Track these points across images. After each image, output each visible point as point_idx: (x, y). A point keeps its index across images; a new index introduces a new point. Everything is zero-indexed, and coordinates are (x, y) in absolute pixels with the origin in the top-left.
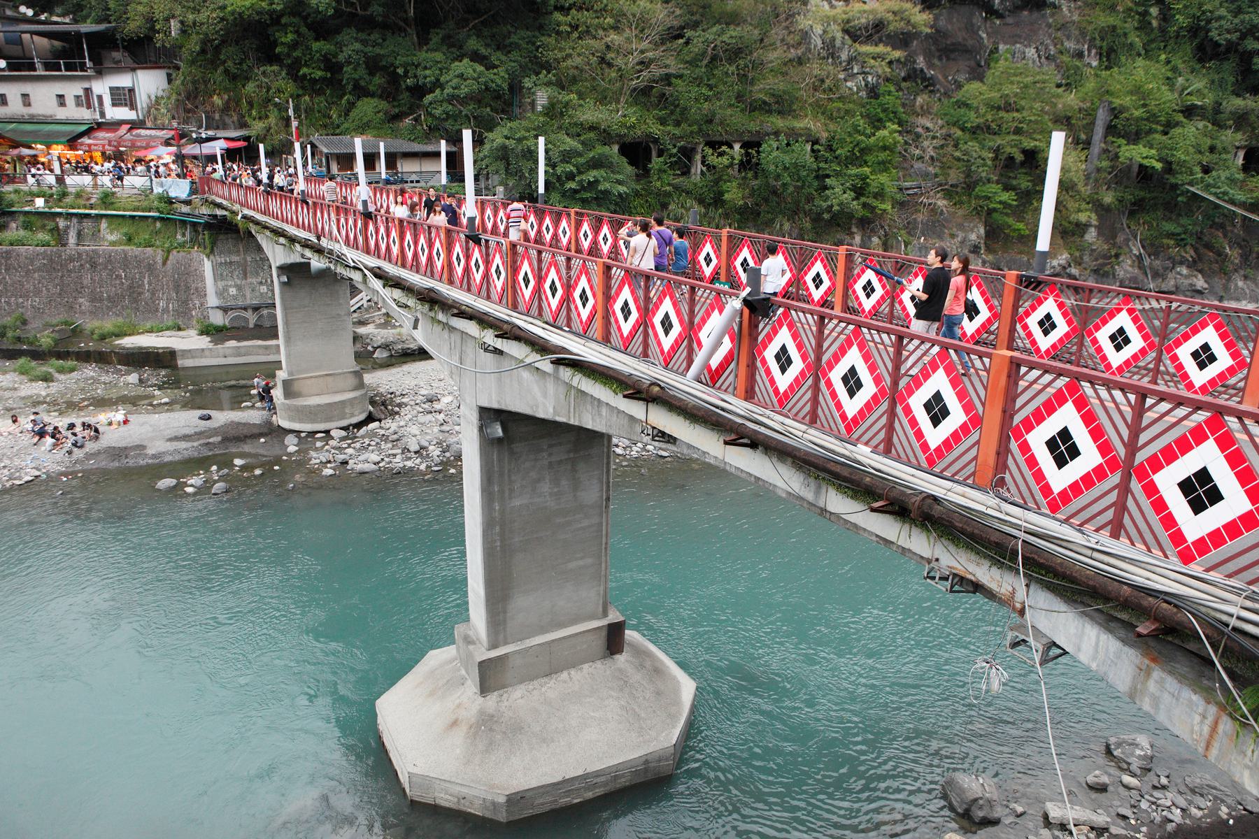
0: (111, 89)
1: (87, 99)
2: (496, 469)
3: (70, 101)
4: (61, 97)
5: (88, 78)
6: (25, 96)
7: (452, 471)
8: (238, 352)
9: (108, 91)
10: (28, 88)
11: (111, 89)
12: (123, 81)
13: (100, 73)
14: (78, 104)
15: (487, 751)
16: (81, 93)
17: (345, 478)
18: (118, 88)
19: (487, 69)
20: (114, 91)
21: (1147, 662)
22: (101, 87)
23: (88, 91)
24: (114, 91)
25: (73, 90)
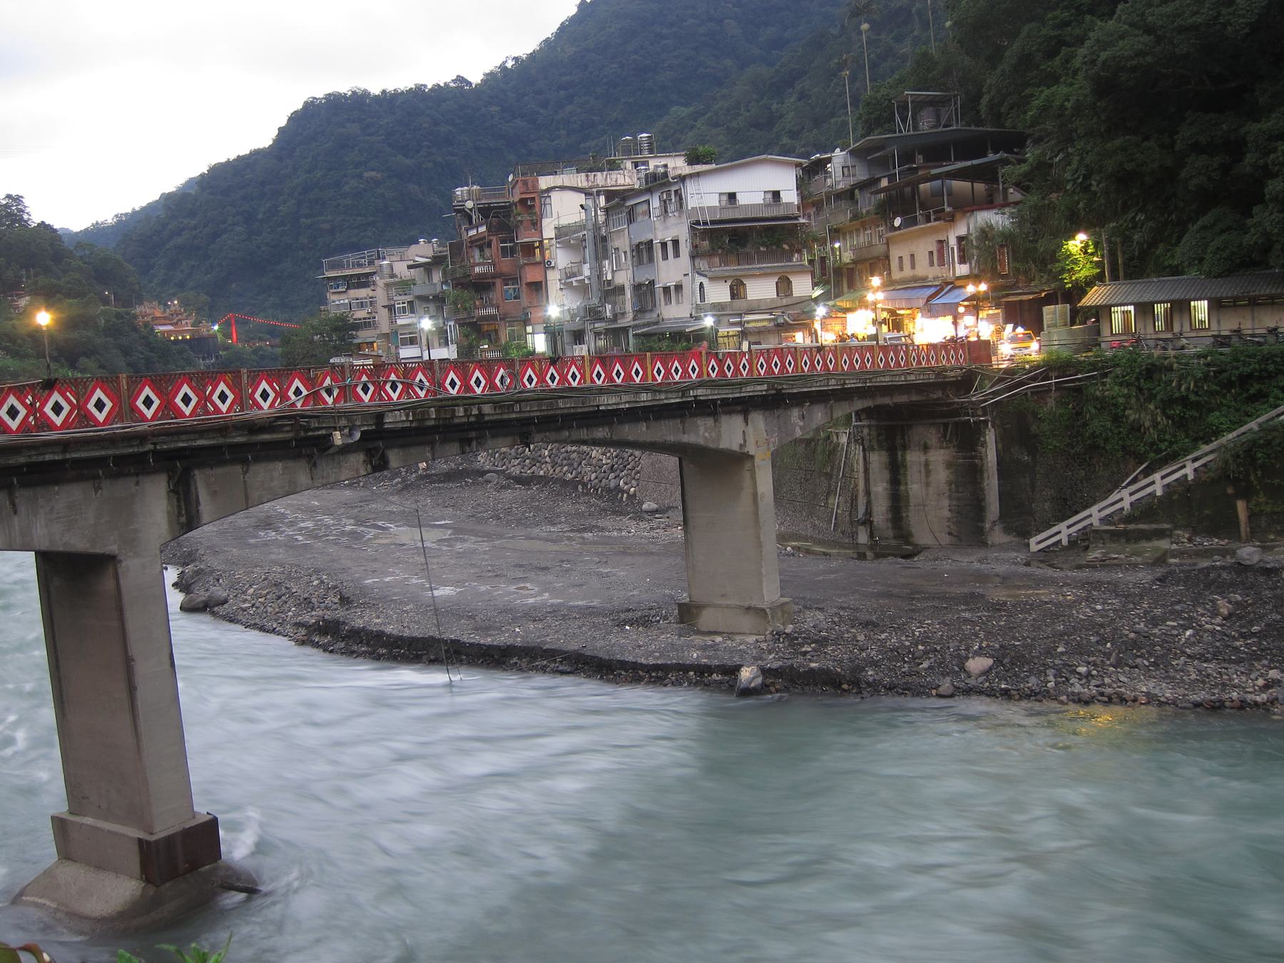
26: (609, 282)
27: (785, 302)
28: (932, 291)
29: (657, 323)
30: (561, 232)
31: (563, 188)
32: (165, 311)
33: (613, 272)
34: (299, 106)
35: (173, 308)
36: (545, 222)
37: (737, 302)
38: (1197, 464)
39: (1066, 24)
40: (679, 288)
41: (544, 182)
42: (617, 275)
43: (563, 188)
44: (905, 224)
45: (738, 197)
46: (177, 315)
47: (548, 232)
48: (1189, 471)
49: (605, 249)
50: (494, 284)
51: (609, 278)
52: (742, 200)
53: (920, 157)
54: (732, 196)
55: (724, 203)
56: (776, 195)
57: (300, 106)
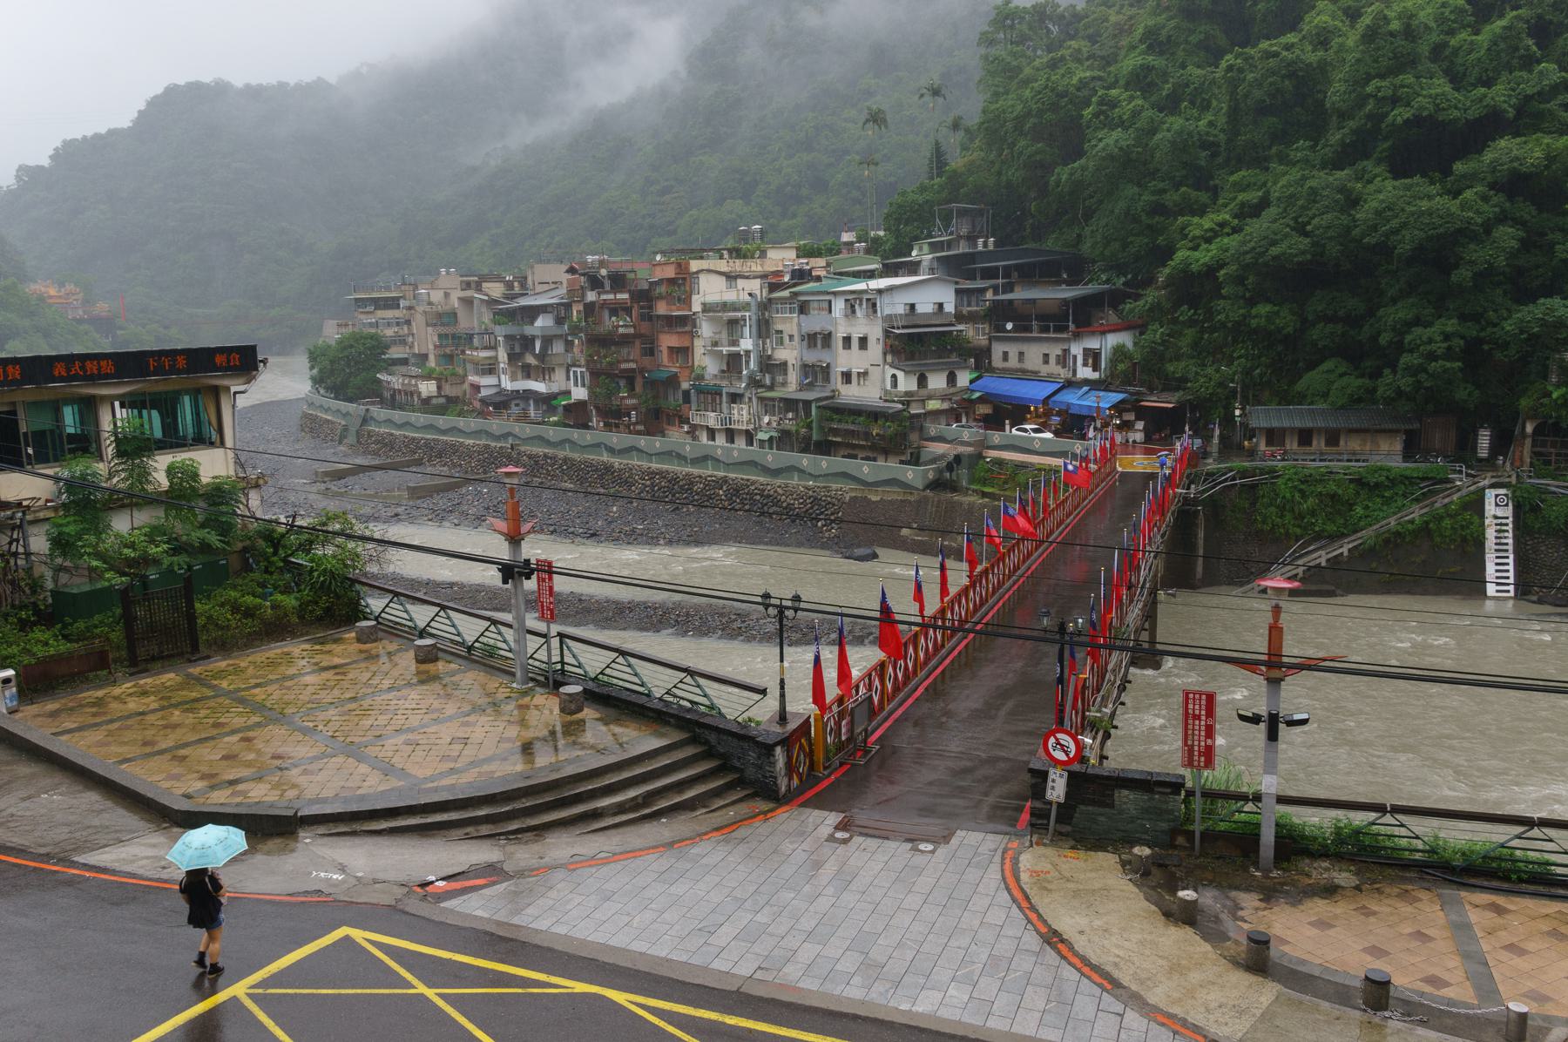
0: (1085, 349)
1: (1063, 359)
2: (322, 874)
3: (1052, 360)
4: (1046, 356)
5: (1068, 340)
6: (1021, 354)
7: (1484, 441)
8: (1500, 549)
9: (1081, 352)
10: (1024, 347)
11: (1085, 350)
12: (1093, 344)
13: (1077, 336)
14: (1058, 363)
15: (1342, 407)
16: (1060, 353)
17: (105, 562)
18: (1090, 349)
19: (1425, 327)
20: (1087, 352)
21: (594, 332)
22: (1076, 349)
23: (1066, 352)
24: (1087, 352)
25: (1055, 351)
26: (769, 357)
27: (952, 390)
28: (1057, 386)
29: (833, 397)
30: (707, 308)
31: (709, 271)
32: (60, 291)
33: (773, 349)
34: (159, 90)
35: (1278, 534)
36: (695, 298)
37: (923, 392)
38: (1351, 546)
39: (1164, 191)
40: (865, 374)
41: (695, 265)
42: (776, 351)
43: (709, 271)
44: (1015, 329)
45: (917, 307)
46: (73, 294)
47: (697, 307)
48: (1345, 550)
49: (768, 330)
50: (634, 342)
51: (769, 353)
52: (920, 309)
53: (1016, 273)
54: (912, 306)
55: (907, 312)
56: (941, 305)
57: (160, 91)
